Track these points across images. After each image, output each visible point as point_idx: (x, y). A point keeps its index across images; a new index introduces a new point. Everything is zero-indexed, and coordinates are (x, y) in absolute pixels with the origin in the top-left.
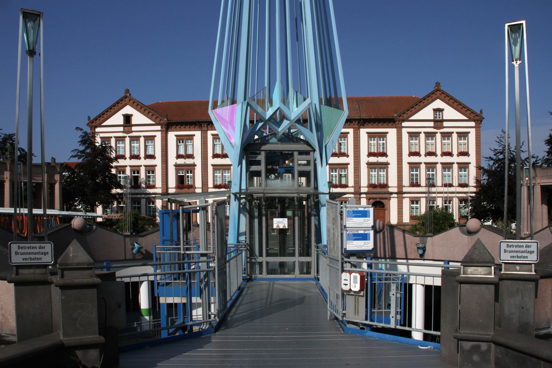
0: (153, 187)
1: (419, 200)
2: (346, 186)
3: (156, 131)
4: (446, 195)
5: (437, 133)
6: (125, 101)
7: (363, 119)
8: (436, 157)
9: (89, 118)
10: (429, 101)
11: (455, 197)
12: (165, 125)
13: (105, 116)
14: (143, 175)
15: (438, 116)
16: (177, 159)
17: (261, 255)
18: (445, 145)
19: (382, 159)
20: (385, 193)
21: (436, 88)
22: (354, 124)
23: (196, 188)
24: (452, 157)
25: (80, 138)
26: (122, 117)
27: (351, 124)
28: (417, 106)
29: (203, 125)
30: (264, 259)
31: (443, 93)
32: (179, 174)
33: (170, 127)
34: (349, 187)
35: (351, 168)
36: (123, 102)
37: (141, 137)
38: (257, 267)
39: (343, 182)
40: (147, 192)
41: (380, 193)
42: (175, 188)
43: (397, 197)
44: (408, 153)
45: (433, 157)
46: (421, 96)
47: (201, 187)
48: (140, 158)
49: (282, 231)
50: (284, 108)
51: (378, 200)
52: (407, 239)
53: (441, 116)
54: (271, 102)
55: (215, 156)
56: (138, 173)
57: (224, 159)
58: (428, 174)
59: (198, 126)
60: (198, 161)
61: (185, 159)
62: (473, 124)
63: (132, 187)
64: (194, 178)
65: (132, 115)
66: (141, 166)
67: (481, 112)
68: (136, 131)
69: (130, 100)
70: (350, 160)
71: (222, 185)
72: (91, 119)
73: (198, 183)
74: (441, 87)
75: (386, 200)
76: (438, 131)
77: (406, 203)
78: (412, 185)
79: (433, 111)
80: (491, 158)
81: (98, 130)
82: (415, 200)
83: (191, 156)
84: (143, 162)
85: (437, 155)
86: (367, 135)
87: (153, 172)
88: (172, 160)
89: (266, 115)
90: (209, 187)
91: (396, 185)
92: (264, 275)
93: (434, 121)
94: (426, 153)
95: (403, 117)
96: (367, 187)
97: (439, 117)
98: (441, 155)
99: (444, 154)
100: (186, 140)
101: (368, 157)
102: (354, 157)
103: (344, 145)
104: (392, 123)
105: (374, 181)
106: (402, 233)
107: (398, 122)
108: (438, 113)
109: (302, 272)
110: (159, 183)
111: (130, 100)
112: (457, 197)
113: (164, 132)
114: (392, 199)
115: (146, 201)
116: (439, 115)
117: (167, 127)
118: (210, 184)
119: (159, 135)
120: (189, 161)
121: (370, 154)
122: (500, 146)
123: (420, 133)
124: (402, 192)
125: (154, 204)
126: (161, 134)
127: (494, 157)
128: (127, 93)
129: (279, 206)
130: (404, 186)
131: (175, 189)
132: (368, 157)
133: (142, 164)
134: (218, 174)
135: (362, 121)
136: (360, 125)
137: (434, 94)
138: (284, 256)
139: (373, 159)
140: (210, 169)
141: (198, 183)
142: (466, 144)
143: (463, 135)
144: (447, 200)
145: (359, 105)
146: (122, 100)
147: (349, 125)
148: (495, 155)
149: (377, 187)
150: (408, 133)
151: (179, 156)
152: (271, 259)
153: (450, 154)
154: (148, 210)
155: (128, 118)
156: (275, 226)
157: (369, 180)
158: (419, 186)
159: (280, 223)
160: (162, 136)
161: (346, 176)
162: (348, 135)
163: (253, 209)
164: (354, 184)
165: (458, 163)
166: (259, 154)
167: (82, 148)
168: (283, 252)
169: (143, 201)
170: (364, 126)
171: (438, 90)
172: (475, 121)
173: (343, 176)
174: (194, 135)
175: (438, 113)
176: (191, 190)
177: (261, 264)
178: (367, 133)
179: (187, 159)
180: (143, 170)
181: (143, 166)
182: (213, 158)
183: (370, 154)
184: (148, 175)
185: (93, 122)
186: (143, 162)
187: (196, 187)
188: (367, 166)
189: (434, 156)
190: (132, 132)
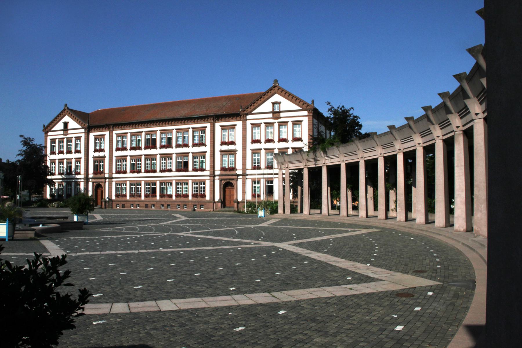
0: (79, 173)
2: (204, 170)
3: (81, 133)
6: (274, 90)
9: (44, 125)
11: (262, 178)
12: (312, 110)
23: (105, 174)
24: (288, 142)
26: (63, 124)
29: (110, 127)
32: (95, 164)
36: (272, 92)
37: (190, 128)
41: (229, 175)
42: (220, 170)
44: (251, 141)
45: (272, 143)
46: (264, 91)
51: (228, 181)
65: (68, 122)
66: (261, 149)
67: (313, 102)
69: (279, 89)
76: (276, 121)
78: (254, 168)
79: (272, 104)
81: (49, 134)
91: (241, 169)
93: (273, 113)
96: (220, 170)
105: (226, 165)
110: (82, 171)
111: (279, 89)
112: (264, 178)
113: (86, 134)
117: (88, 130)
118: (114, 171)
119: (83, 135)
130: (248, 169)
132: (221, 146)
134: (225, 158)
139: (225, 147)
140: (114, 159)
141: (107, 170)
146: (62, 112)
150: (251, 124)
151: (96, 151)
155: (66, 124)
158: (259, 168)
160: (85, 137)
165: (292, 148)
167: (25, 148)
169: (73, 184)
176: (102, 176)
178: (221, 126)
182: (116, 151)
187: (106, 173)
188: (220, 153)
190: (68, 134)
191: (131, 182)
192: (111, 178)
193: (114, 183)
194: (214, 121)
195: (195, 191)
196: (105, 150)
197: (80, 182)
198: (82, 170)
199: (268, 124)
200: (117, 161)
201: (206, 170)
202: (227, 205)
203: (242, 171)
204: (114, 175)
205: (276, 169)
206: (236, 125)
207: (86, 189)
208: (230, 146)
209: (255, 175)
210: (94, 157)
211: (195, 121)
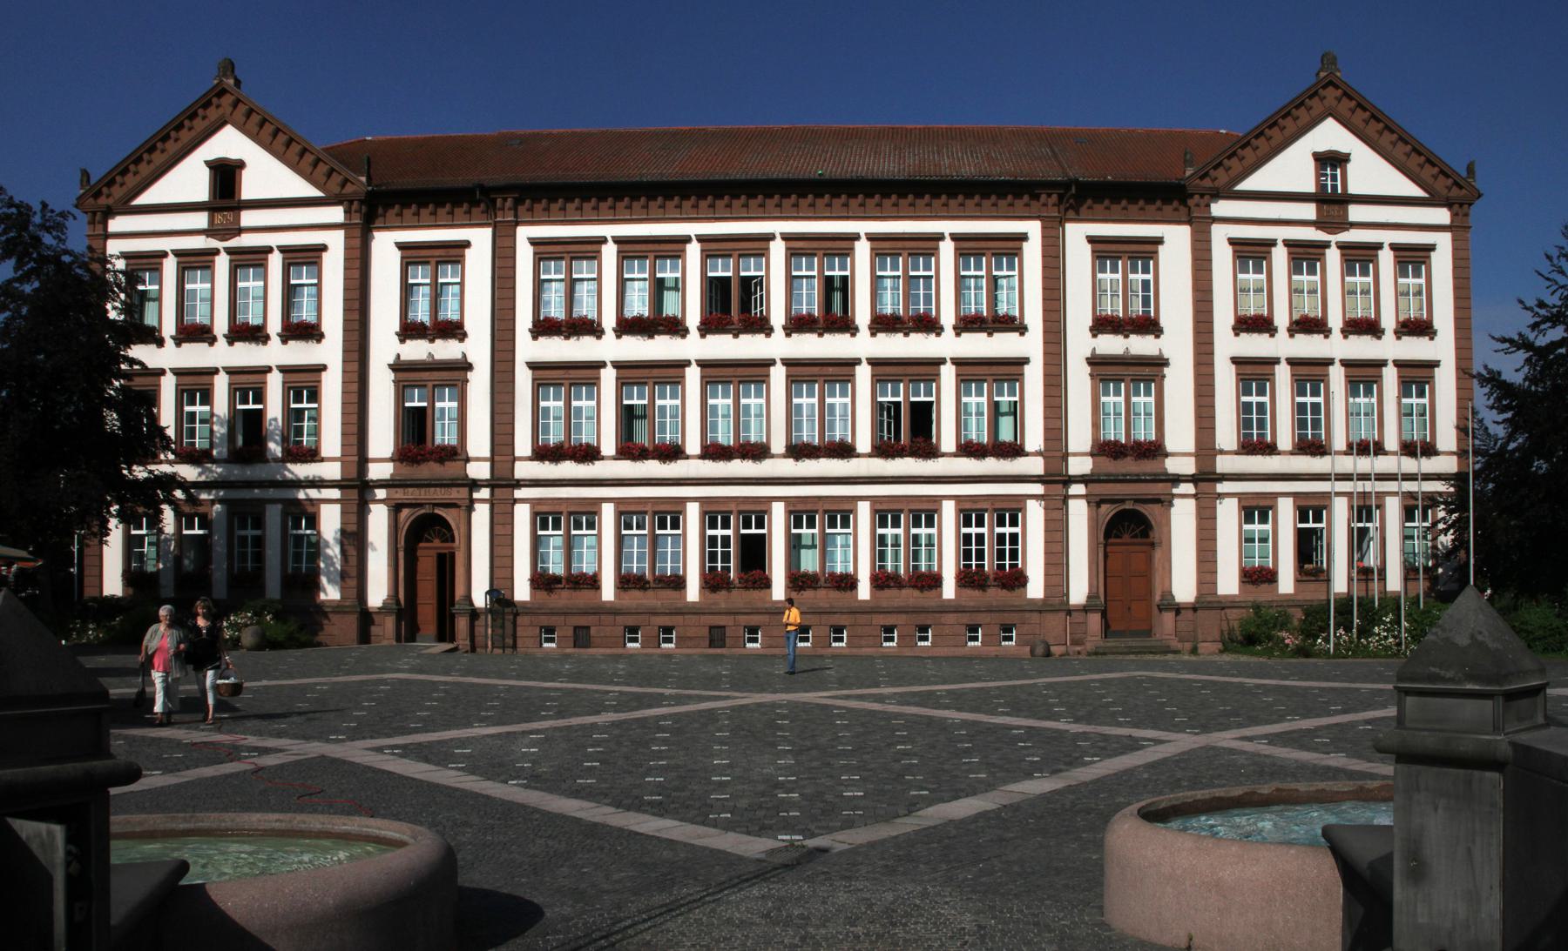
0: (312, 455)
2: (1014, 450)
4: (1360, 486)
9: (85, 174)
12: (362, 202)
16: (402, 341)
19: (1141, 345)
22: (1045, 205)
26: (207, 170)
29: (499, 202)
33: (380, 211)
34: (1027, 455)
35: (1034, 376)
36: (213, 113)
41: (1137, 479)
44: (1231, 321)
47: (487, 454)
51: (1128, 506)
55: (544, 327)
57: (573, 340)
60: (477, 347)
62: (1442, 216)
65: (241, 165)
67: (1470, 170)
70: (1030, 345)
71: (566, 446)
73: (479, 442)
75: (1156, 508)
76: (1333, 238)
77: (1228, 514)
79: (1311, 164)
81: (117, 224)
83: (454, 330)
84: (276, 353)
88: (385, 345)
90: (517, 454)
94: (1292, 323)
96: (1092, 455)
103: (1011, 288)
105: (1115, 432)
107: (1197, 197)
110: (331, 441)
113: (357, 232)
114: (1176, 501)
116: (1334, 178)
118: (523, 444)
119: (336, 242)
120: (446, 350)
121: (1102, 325)
124: (1215, 473)
126: (346, 238)
128: (225, 75)
130: (1222, 452)
133: (273, 363)
136: (1066, 210)
139: (1112, 344)
140: (523, 380)
141: (479, 442)
149: (1125, 456)
151: (409, 330)
155: (226, 175)
157: (1096, 426)
161: (1016, 411)
162: (467, 251)
164: (1046, 440)
172: (1448, 204)
176: (449, 470)
182: (535, 338)
183: (1102, 325)
186: (276, 353)
188: (1088, 369)
190: (240, 231)
193: (522, 515)
194: (1059, 212)
198: (331, 441)
201: (324, 454)
203: (1193, 459)
204: (523, 470)
207: (354, 538)
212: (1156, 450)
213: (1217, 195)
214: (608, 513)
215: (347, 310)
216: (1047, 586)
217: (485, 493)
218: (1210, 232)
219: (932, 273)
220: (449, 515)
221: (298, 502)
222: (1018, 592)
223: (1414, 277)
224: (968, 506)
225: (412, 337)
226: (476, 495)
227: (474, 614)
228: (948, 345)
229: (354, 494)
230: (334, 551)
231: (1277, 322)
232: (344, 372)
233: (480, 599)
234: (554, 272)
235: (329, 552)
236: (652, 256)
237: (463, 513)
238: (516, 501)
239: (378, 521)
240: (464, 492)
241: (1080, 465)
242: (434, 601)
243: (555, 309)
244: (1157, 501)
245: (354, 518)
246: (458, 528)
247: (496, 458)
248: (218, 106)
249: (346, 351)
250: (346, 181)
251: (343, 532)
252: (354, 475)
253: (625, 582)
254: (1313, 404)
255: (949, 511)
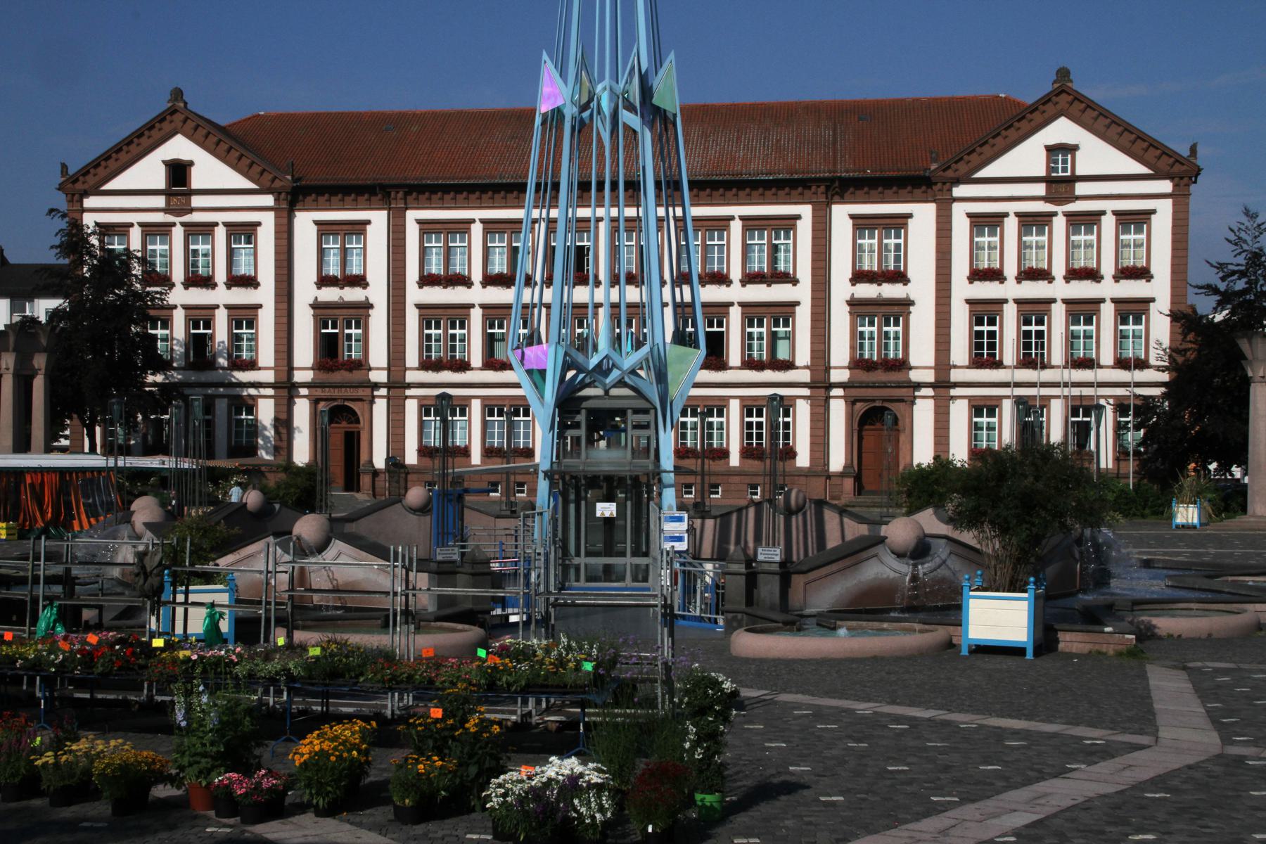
0: (252, 365)
1: (997, 406)
2: (789, 365)
4: (1076, 391)
5: (1055, 214)
7: (840, 179)
8: (1050, 282)
9: (64, 167)
10: (1046, 115)
12: (287, 193)
13: (112, 164)
14: (221, 331)
15: (1060, 166)
16: (319, 288)
17: (578, 554)
18: (1079, 247)
19: (891, 291)
20: (899, 386)
21: (1056, 86)
22: (815, 193)
24: (1099, 282)
25: (59, 236)
26: (163, 167)
27: (806, 192)
28: (999, 139)
29: (393, 194)
30: (582, 560)
31: (1078, 98)
32: (323, 331)
33: (301, 198)
34: (797, 368)
35: (803, 316)
36: (166, 126)
37: (216, 224)
38: (572, 572)
39: (783, 354)
40: (234, 380)
41: (885, 386)
43: (932, 397)
46: (1029, 98)
47: (385, 365)
48: (214, 286)
49: (608, 521)
50: (615, 356)
51: (878, 404)
52: (846, 527)
53: (1069, 166)
54: (595, 348)
55: (427, 280)
56: (208, 325)
57: (449, 289)
58: (1025, 332)
59: (380, 196)
60: (377, 292)
61: (342, 288)
62: (1166, 186)
63: (190, 366)
64: (365, 339)
65: (191, 163)
66: (217, 307)
67: (1193, 150)
68: (202, 209)
70: (802, 293)
71: (445, 361)
72: (72, 171)
73: (378, 355)
74: (1071, 81)
75: (901, 406)
77: (959, 413)
79: (1044, 153)
80: (1214, 290)
81: (89, 202)
82: (985, 406)
83: (360, 281)
84: (222, 296)
85: (1053, 278)
86: (851, 221)
87: (250, 325)
88: (306, 290)
89: (588, 363)
90: (408, 365)
91: (932, 363)
92: (582, 583)
93: (1048, 180)
94: (1020, 273)
95: (956, 170)
96: (849, 368)
97: (1065, 170)
98: (1065, 278)
99: (1074, 274)
100: (345, 234)
101: (853, 285)
102: (813, 283)
103: (787, 251)
104: (924, 188)
105: (870, 352)
106: (837, 516)
107: (939, 185)
108: (1060, 157)
109: (635, 579)
110: (266, 354)
113: (285, 214)
114: (918, 401)
115: (229, 407)
116: (1065, 162)
118: (412, 358)
119: (268, 221)
120: (353, 294)
121: (859, 277)
122: (1240, 254)
123: (1006, 215)
124: (949, 382)
125: (252, 415)
126: (276, 217)
127: (1222, 286)
128: (176, 99)
129: (605, 485)
130: (955, 367)
131: (311, 372)
132: (853, 285)
133: (221, 302)
135: (837, 184)
136: (833, 196)
137: (1050, 104)
138: (611, 556)
139: (867, 291)
140: (412, 319)
141: (378, 355)
142: (1142, 244)
143: (1134, 220)
144: (1082, 409)
145: (835, 131)
146: (161, 119)
147: (801, 194)
148: (1223, 279)
149: (876, 369)
150: (970, 215)
151: (324, 281)
152: (593, 561)
153: (1092, 275)
154: (234, 429)
155: (178, 172)
156: (598, 514)
159: (606, 509)
161: (790, 337)
162: (368, 227)
163: (568, 490)
164: (812, 358)
165: (1114, 301)
166: (578, 412)
168: (609, 551)
170: (842, 197)
171: (1063, 91)
172: (1171, 178)
173: (780, 335)
174: (368, 222)
175: (1060, 157)
176: (356, 376)
177: (577, 568)
179: (346, 288)
180: (221, 319)
181: (222, 308)
182: (421, 287)
183: (859, 277)
184: (235, 331)
185: (76, 181)
186: (222, 296)
187: (372, 364)
188: (848, 308)
189: (1043, 279)
190: (192, 210)
191: (487, 403)
192: (397, 386)
193: (411, 407)
194: (827, 198)
195: (750, 436)
196: (369, 279)
197: (254, 398)
198: (266, 354)
199: (1030, 219)
200: (425, 322)
202: (867, 487)
203: (933, 371)
204: (411, 377)
205: (1058, 367)
206: (369, 222)
207: (284, 424)
208: (885, 285)
209: (1032, 385)
210: (316, 306)
211: (434, 197)
212: (901, 365)
213: (958, 182)
214: (476, 406)
215: (277, 267)
216: (812, 459)
217: (383, 392)
218: (951, 209)
219: (725, 242)
220: (355, 406)
221: (241, 397)
222: (788, 463)
223: (758, 327)
224: (749, 403)
225: (327, 285)
226: (376, 393)
227: (376, 473)
228: (736, 293)
229: (284, 393)
230: (270, 433)
231: (1006, 273)
232: (276, 309)
233: (379, 462)
234: (435, 244)
235: (267, 433)
236: (509, 231)
237: (366, 406)
238: (407, 397)
239: (302, 411)
240: (368, 391)
241: (839, 375)
242: (342, 464)
243: (436, 267)
244: (900, 400)
245: (285, 408)
246: (363, 415)
247: (392, 368)
248: (171, 122)
249: (277, 295)
250: (275, 178)
251: (276, 419)
252: (285, 379)
253: (488, 452)
254: (1037, 332)
255: (735, 406)
